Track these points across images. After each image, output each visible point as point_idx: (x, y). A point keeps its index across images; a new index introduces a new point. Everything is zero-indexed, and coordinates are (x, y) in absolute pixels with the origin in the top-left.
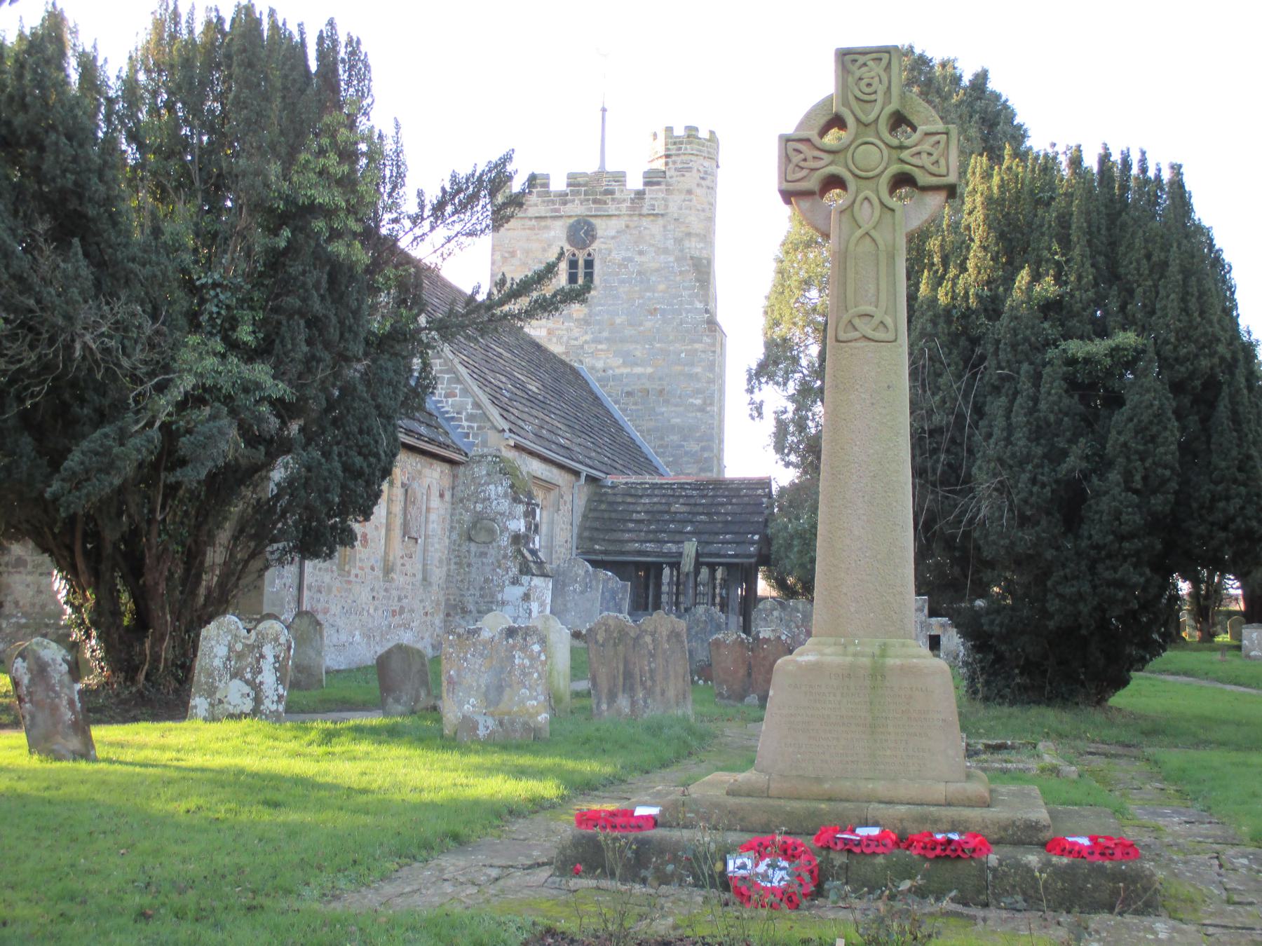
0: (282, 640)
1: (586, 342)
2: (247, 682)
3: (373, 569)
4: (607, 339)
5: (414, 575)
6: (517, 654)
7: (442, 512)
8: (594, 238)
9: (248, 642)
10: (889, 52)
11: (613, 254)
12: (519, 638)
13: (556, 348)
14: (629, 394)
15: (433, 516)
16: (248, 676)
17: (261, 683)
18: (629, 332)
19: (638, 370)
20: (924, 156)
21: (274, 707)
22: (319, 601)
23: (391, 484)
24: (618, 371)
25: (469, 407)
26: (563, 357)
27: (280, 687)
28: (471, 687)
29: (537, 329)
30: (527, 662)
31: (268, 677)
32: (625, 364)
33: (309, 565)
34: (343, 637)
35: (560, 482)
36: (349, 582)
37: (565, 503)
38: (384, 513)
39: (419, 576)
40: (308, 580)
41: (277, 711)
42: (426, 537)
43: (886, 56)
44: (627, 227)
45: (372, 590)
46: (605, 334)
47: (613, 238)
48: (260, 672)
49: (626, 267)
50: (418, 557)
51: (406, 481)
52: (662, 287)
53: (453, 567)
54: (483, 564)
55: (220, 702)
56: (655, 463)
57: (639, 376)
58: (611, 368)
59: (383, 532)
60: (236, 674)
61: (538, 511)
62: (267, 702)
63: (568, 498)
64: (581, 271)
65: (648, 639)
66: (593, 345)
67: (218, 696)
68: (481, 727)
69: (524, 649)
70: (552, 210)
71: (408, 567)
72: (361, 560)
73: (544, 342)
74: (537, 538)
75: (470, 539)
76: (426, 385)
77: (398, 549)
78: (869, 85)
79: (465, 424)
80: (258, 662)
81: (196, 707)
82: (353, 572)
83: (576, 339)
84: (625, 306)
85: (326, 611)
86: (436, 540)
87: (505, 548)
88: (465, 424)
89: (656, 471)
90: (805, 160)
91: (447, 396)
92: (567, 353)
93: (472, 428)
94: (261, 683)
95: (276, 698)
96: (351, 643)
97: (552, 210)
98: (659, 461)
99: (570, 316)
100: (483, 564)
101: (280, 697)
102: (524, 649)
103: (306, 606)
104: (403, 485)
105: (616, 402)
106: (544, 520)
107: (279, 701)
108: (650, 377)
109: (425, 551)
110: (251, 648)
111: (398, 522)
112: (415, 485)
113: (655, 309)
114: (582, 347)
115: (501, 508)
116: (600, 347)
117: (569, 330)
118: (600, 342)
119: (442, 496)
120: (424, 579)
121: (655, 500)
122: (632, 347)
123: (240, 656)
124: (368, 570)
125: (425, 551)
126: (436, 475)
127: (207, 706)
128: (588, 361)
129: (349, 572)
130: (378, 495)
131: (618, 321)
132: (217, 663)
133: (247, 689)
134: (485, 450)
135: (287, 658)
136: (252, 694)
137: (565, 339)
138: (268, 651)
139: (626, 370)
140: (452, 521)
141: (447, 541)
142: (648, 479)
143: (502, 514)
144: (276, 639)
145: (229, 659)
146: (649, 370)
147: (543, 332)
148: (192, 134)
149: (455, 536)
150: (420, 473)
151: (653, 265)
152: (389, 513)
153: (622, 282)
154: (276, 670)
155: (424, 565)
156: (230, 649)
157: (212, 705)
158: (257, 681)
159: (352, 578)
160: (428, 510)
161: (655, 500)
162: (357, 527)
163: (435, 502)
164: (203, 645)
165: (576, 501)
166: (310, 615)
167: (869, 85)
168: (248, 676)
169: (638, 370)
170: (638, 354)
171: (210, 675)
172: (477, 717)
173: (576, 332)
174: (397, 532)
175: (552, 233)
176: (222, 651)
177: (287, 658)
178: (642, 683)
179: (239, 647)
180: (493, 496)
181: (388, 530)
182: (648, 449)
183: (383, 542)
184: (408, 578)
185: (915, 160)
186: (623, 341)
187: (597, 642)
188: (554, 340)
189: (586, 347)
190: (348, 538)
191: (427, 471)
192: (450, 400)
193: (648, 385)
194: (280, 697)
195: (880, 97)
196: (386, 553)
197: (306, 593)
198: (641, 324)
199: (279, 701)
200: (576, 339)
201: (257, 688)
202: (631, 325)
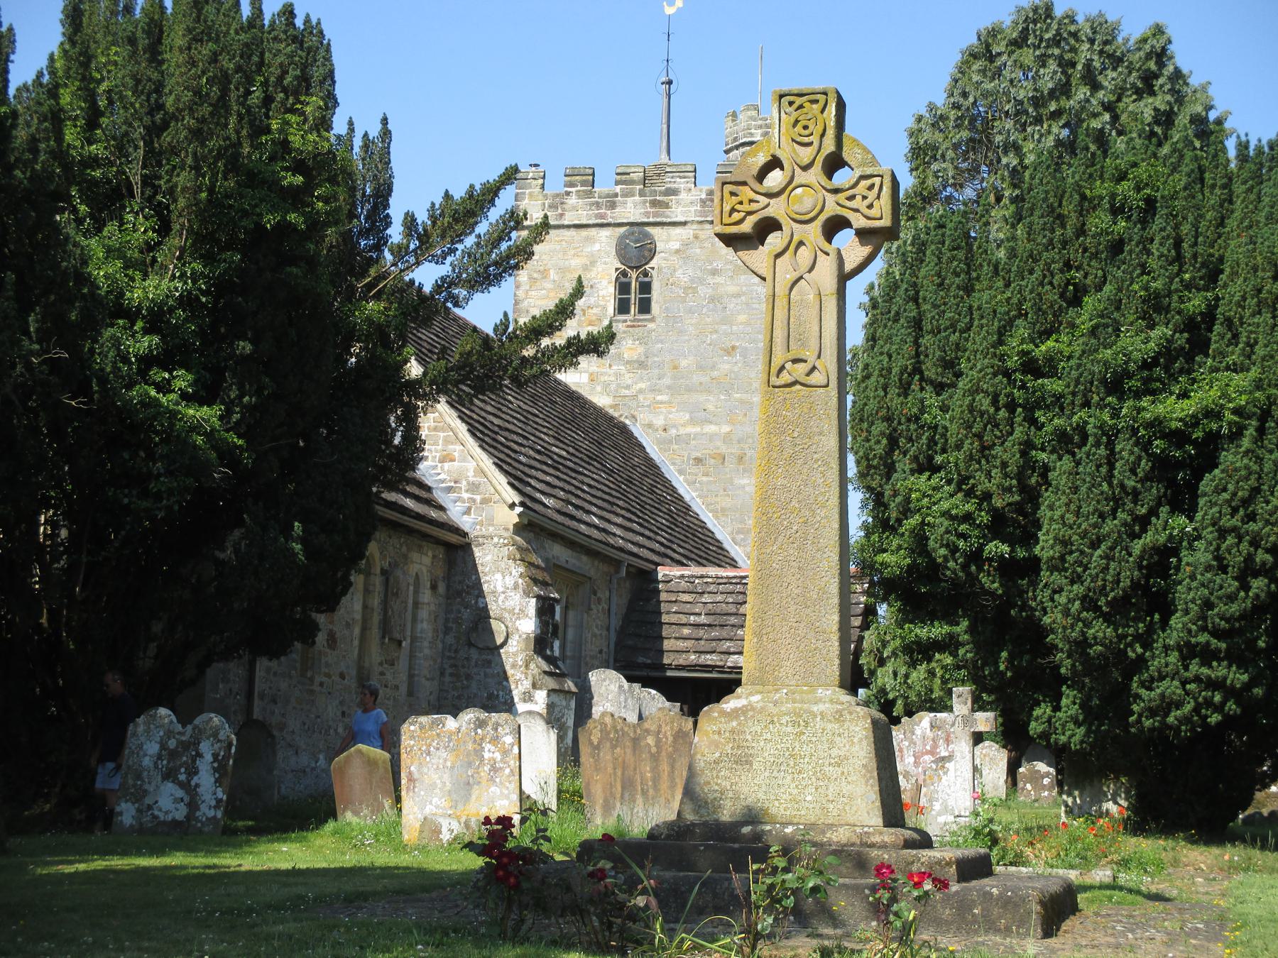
0: (222, 736)
1: (641, 391)
2: (182, 785)
3: (342, 676)
4: (669, 387)
5: (397, 687)
6: (487, 746)
7: (433, 607)
8: (653, 253)
9: (184, 738)
10: (826, 94)
11: (679, 273)
12: (489, 728)
13: (601, 400)
14: (698, 461)
15: (424, 614)
16: (182, 777)
17: (197, 785)
18: (697, 378)
19: (711, 429)
20: (859, 198)
21: (211, 813)
22: (273, 713)
23: (368, 574)
24: (682, 431)
25: (471, 473)
26: (611, 411)
27: (219, 789)
28: (433, 786)
29: (570, 378)
30: (498, 756)
31: (206, 780)
32: (692, 421)
33: (262, 664)
34: (304, 760)
35: (592, 573)
36: (312, 692)
37: (599, 600)
38: (358, 607)
39: (404, 689)
40: (259, 686)
41: (215, 817)
42: (414, 639)
43: (821, 98)
44: (696, 237)
45: (342, 703)
46: (667, 381)
47: (677, 251)
48: (196, 773)
49: (695, 290)
50: (403, 664)
51: (386, 566)
52: (742, 318)
53: (447, 679)
54: (486, 675)
55: (150, 807)
56: (733, 554)
57: (712, 437)
58: (674, 426)
59: (357, 631)
60: (169, 775)
61: (558, 609)
62: (204, 808)
63: (603, 594)
64: (633, 297)
65: (650, 740)
66: (650, 396)
67: (148, 801)
68: (444, 830)
69: (495, 740)
70: (597, 216)
71: (389, 676)
72: (327, 665)
73: (585, 392)
74: (557, 644)
75: (470, 645)
76: (412, 447)
77: (375, 655)
78: (805, 127)
79: (466, 496)
80: (194, 761)
81: (121, 814)
82: (318, 679)
83: (628, 387)
84: (694, 342)
85: (282, 727)
86: (426, 644)
87: (515, 654)
88: (466, 496)
89: (733, 564)
90: (741, 203)
91: (442, 461)
92: (615, 406)
93: (474, 501)
94: (197, 785)
95: (213, 803)
96: (313, 769)
97: (597, 216)
98: (735, 551)
99: (619, 357)
100: (486, 675)
101: (219, 801)
102: (495, 740)
103: (257, 714)
104: (384, 572)
105: (681, 472)
106: (571, 621)
107: (216, 807)
108: (727, 438)
109: (412, 656)
110: (186, 746)
111: (376, 619)
112: (399, 573)
113: (733, 348)
114: (635, 397)
115: (509, 604)
116: (659, 398)
117: (618, 375)
118: (660, 392)
119: (434, 587)
120: (411, 693)
121: (719, 598)
122: (702, 398)
123: (173, 754)
124: (336, 678)
125: (412, 656)
126: (427, 560)
127: (133, 812)
128: (643, 417)
129: (312, 679)
130: (348, 585)
131: (684, 363)
132: (147, 762)
133: (180, 793)
134: (491, 529)
135: (227, 757)
136: (187, 799)
137: (613, 387)
138: (206, 748)
139: (691, 429)
140: (447, 620)
141: (440, 646)
142: (712, 571)
143: (511, 611)
144: (215, 735)
145: (160, 757)
146: (726, 429)
147: (585, 378)
148: (181, 766)
149: (450, 639)
150: (405, 557)
151: (732, 289)
152: (365, 607)
153: (690, 311)
154: (215, 770)
155: (411, 676)
156: (163, 746)
157: (139, 811)
158: (193, 783)
159: (316, 688)
160: (416, 604)
161: (719, 598)
162: (321, 619)
163: (426, 596)
164: (131, 743)
165: (615, 599)
166: (262, 726)
167: (805, 127)
168: (182, 777)
169: (711, 429)
170: (710, 407)
171: (139, 776)
172: (441, 820)
173: (628, 378)
174: (375, 632)
175: (597, 247)
176: (153, 748)
177: (227, 757)
178: (644, 793)
179: (172, 744)
180: (500, 589)
181: (364, 629)
182: (722, 534)
183: (356, 643)
184: (388, 690)
185: (848, 204)
186: (689, 390)
187: (591, 743)
188: (599, 389)
189: (641, 397)
190: (307, 632)
191: (415, 556)
192: (446, 465)
193: (724, 449)
194: (219, 801)
195: (815, 139)
196: (360, 657)
197: (256, 701)
198: (713, 367)
199: (216, 807)
200: (628, 387)
201: (191, 791)
202: (701, 368)
